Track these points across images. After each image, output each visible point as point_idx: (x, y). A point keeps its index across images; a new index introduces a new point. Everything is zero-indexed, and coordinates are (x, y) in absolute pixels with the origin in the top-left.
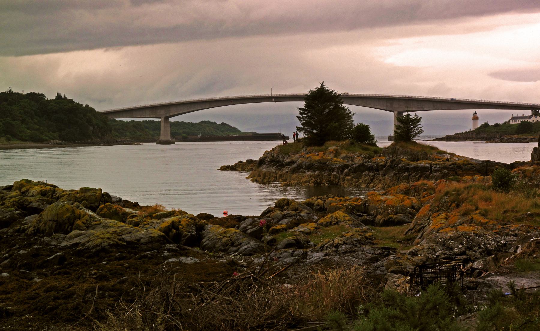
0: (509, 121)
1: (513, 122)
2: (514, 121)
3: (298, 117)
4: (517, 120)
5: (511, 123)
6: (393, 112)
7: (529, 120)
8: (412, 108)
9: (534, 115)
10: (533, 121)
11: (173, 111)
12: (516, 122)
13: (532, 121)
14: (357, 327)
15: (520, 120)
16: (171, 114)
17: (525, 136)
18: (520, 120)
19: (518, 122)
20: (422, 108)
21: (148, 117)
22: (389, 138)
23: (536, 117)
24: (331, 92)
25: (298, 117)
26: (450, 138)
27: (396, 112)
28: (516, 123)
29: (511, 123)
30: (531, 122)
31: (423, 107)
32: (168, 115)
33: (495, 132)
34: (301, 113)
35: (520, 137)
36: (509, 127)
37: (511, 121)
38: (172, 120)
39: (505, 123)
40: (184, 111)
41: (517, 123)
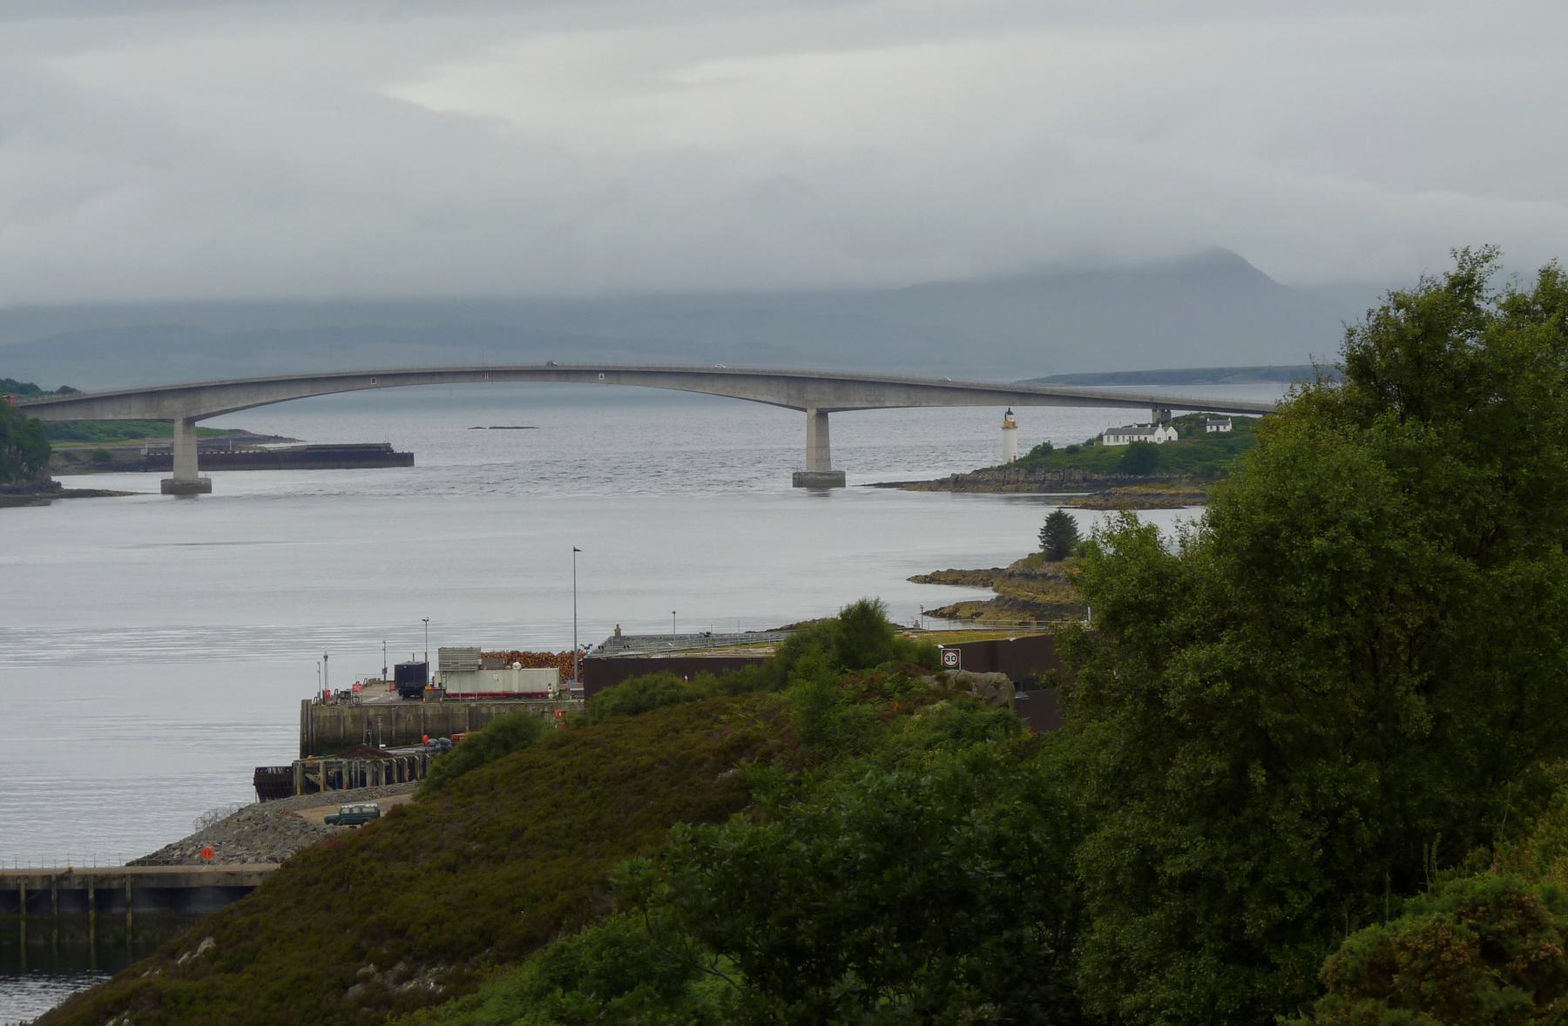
0: (1100, 437)
1: (1109, 442)
2: (1112, 437)
3: (1039, 536)
4: (1121, 437)
5: (1105, 443)
6: (805, 410)
7: (1150, 439)
8: (854, 400)
9: (1160, 425)
10: (1159, 439)
11: (208, 402)
12: (1118, 440)
13: (1156, 440)
14: (1382, 499)
15: (1127, 437)
16: (203, 412)
17: (1158, 488)
18: (1127, 437)
19: (1124, 441)
20: (879, 401)
21: (785, 403)
22: (797, 477)
23: (1166, 430)
24: (1066, 515)
25: (1039, 536)
26: (962, 480)
27: (813, 412)
28: (1117, 444)
29: (1105, 443)
30: (1155, 443)
31: (882, 399)
32: (193, 414)
33: (1071, 467)
34: (1042, 533)
35: (1145, 492)
36: (1101, 453)
37: (1105, 438)
38: (198, 424)
39: (1090, 442)
40: (240, 405)
41: (1121, 443)
